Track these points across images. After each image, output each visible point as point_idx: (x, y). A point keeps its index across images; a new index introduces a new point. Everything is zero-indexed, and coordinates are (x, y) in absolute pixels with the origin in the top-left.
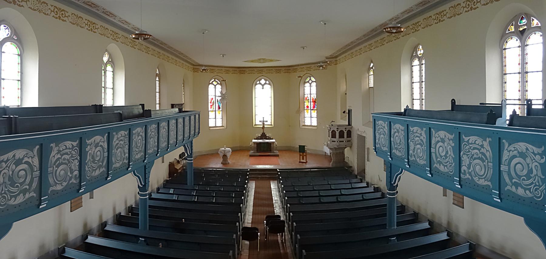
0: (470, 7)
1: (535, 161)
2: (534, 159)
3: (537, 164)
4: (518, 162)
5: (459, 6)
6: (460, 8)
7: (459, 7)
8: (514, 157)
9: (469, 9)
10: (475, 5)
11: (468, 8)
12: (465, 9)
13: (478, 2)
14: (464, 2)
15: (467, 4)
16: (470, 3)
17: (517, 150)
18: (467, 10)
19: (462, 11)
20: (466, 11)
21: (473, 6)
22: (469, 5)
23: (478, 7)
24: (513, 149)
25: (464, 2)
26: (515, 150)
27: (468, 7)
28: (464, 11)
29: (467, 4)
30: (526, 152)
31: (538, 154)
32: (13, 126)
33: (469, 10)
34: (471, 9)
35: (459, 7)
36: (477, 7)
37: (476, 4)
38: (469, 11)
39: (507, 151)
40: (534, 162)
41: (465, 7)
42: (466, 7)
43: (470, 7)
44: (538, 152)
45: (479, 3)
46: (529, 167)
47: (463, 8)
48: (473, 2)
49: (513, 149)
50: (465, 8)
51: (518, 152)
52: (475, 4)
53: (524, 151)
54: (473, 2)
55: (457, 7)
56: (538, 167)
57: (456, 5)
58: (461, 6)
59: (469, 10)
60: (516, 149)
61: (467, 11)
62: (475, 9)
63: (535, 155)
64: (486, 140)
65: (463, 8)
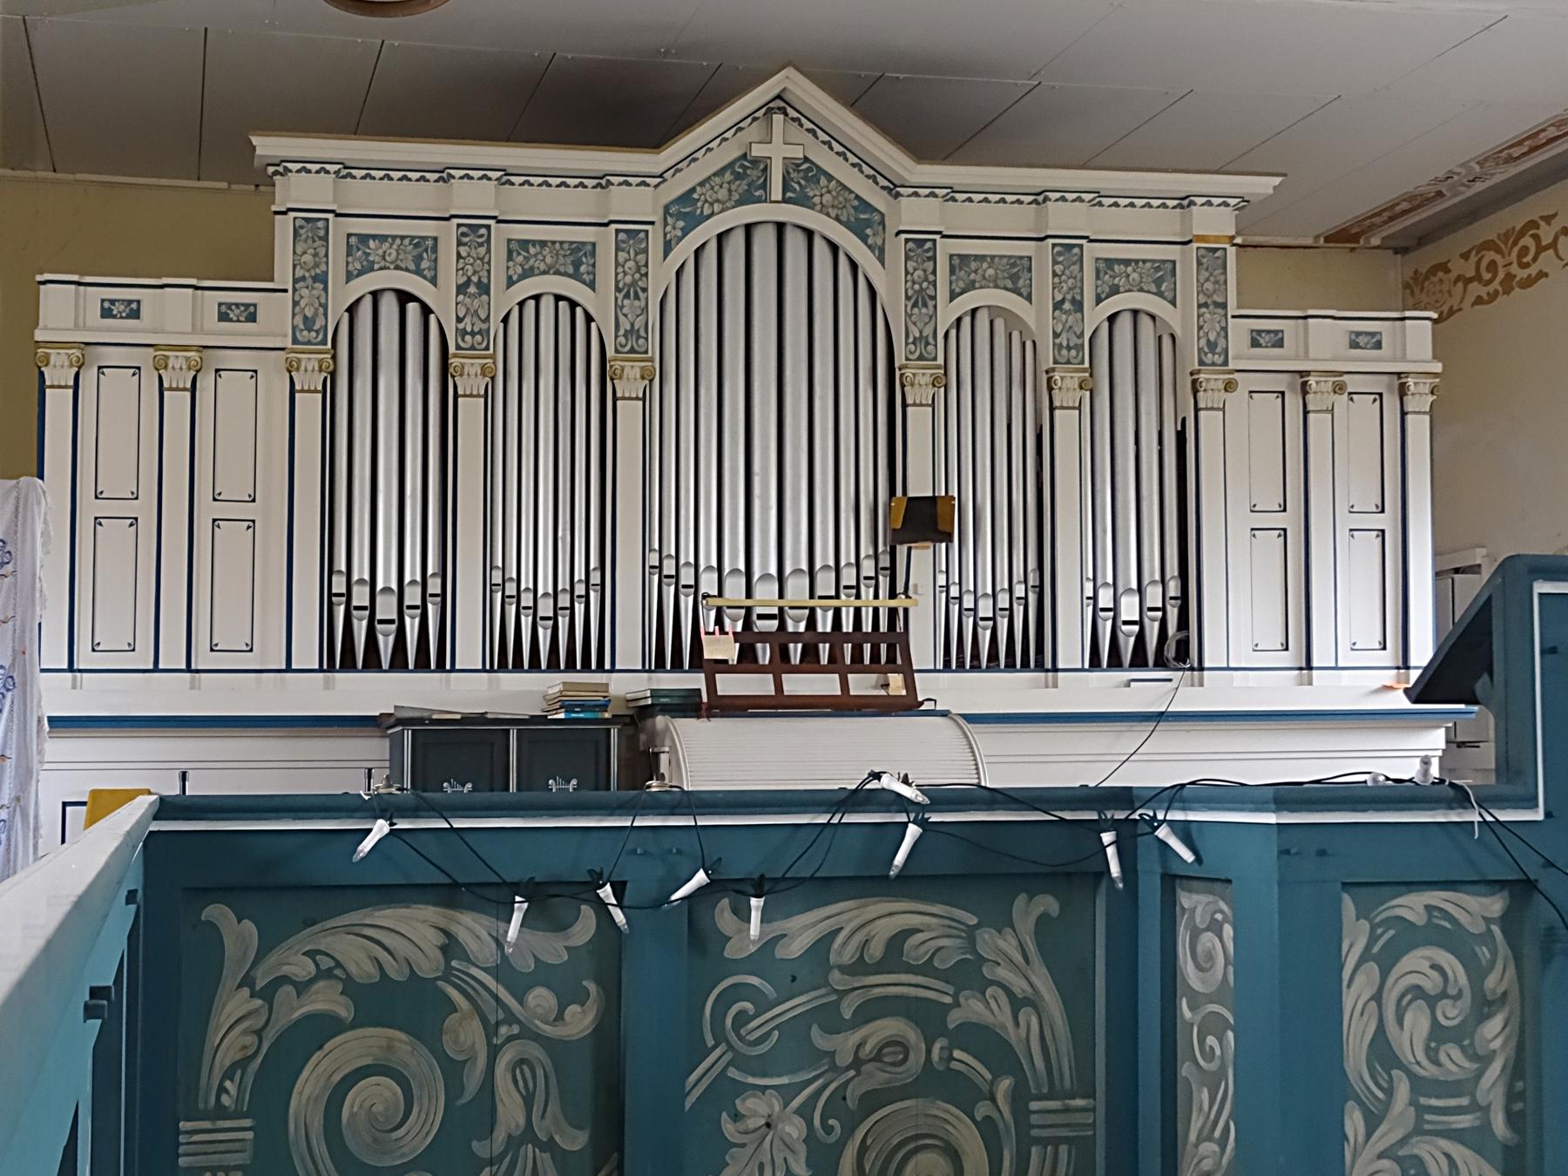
0: (1501, 275)
1: (516, 1029)
2: (511, 1019)
3: (535, 1051)
4: (368, 1061)
5: (1440, 274)
6: (1445, 287)
7: (1441, 281)
8: (321, 1029)
9: (1496, 285)
10: (1527, 265)
11: (1490, 282)
12: (1476, 289)
13: (1546, 248)
14: (1470, 251)
15: (1484, 264)
16: (1498, 258)
17: (338, 972)
18: (1483, 291)
19: (1455, 303)
20: (1479, 301)
21: (1514, 269)
22: (1492, 266)
23: (1546, 275)
24: (307, 968)
25: (1470, 251)
26: (323, 974)
27: (1487, 276)
28: (1470, 299)
29: (1484, 264)
30: (446, 977)
31: (544, 974)
32: (1056, 1073)
33: (1496, 293)
34: (1508, 284)
35: (1441, 281)
36: (1542, 275)
37: (1535, 259)
38: (1493, 297)
39: (246, 991)
40: (510, 1039)
41: (1471, 280)
42: (1478, 277)
43: (1501, 275)
44: (537, 960)
45: (1551, 252)
46: (454, 1087)
47: (1460, 285)
48: (1516, 249)
49: (302, 968)
50: (1468, 276)
51: (350, 987)
52: (1528, 259)
53: (429, 964)
54: (1516, 249)
55: (1427, 283)
56: (893, 1064)
57: (1423, 269)
58: (1453, 275)
59: (1496, 293)
60: (325, 963)
61: (1485, 297)
62: (1528, 283)
63: (520, 985)
64: (1004, 922)
65: (1460, 285)
